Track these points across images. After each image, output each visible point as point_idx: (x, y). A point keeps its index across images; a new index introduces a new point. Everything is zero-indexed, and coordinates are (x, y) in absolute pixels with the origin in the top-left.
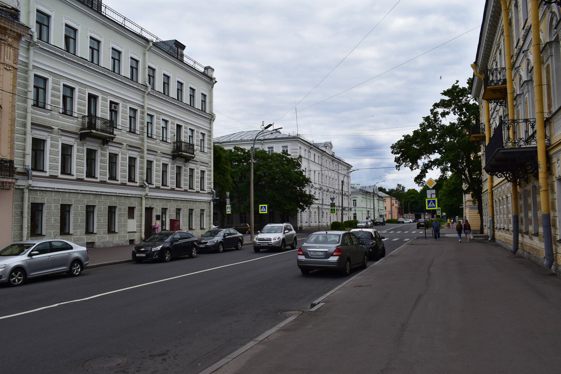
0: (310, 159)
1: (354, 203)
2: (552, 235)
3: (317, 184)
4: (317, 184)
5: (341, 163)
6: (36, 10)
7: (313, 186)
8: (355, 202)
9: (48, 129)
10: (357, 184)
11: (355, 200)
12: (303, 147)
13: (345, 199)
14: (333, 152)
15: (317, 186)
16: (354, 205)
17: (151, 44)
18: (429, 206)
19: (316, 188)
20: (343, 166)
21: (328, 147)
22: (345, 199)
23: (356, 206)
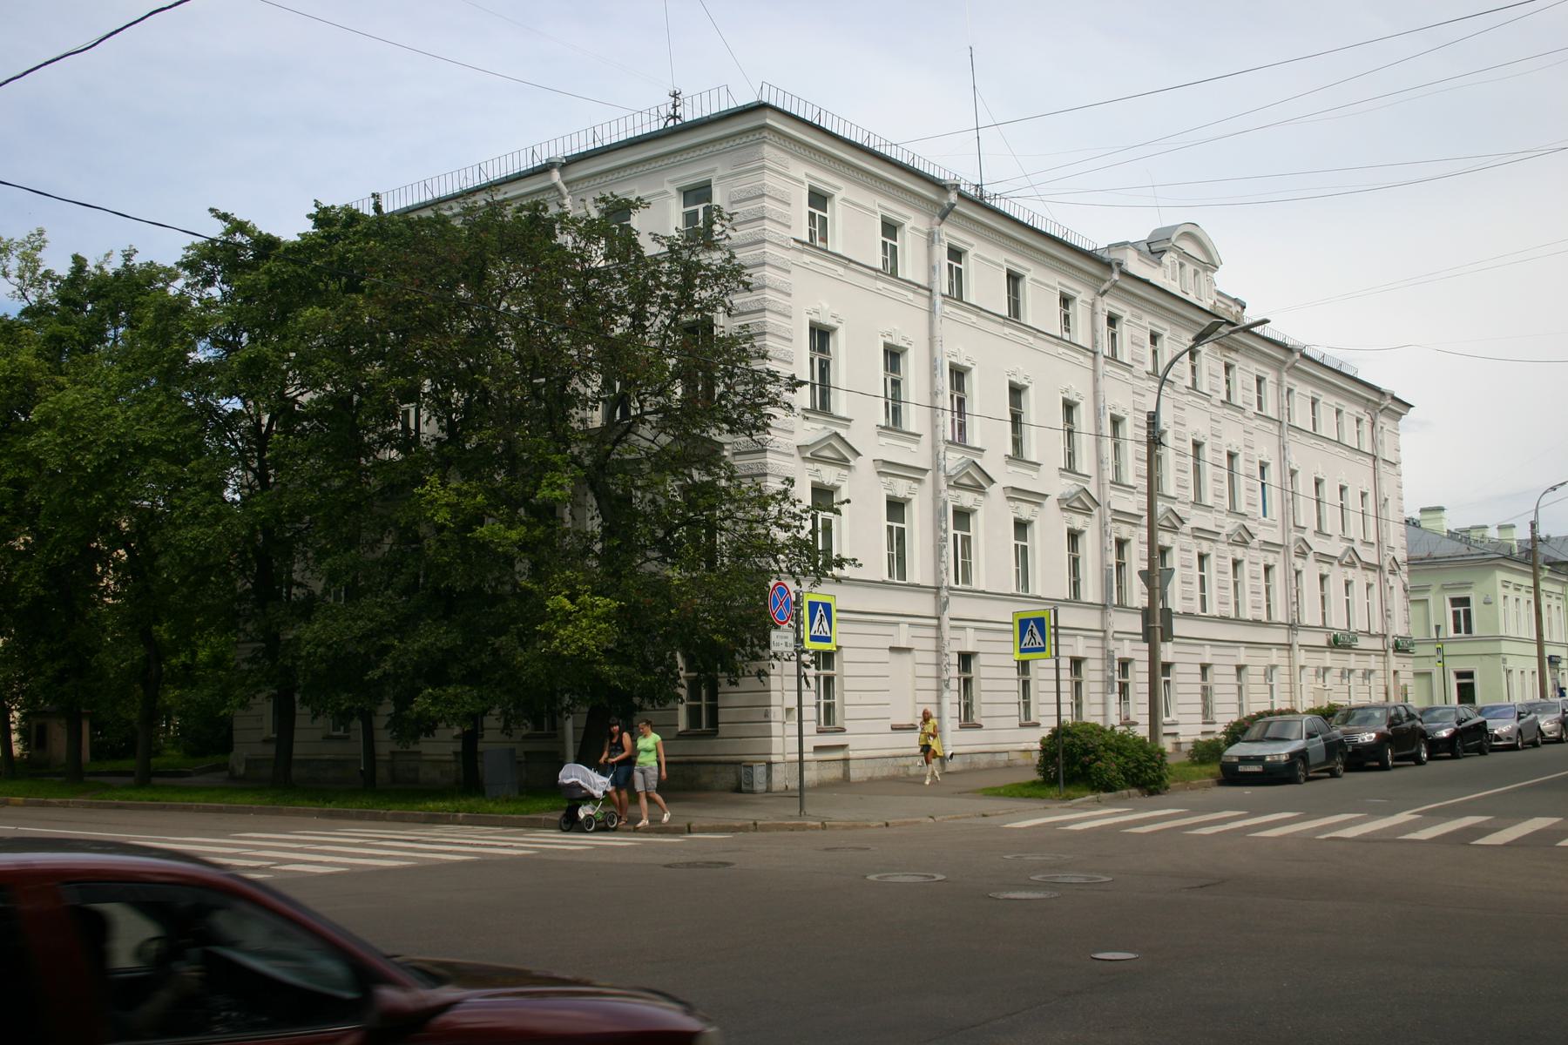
0: (1380, 455)
1: (1456, 614)
2: (1146, 513)
3: (1336, 538)
4: (1336, 538)
5: (1293, 367)
6: (946, 250)
7: (1310, 549)
8: (1461, 609)
9: (1037, 498)
10: (1500, 528)
11: (1465, 601)
12: (1351, 410)
13: (1549, 606)
14: (1236, 301)
15: (1336, 548)
16: (1457, 629)
17: (1297, 356)
18: (1023, 646)
19: (1323, 558)
20: (1348, 400)
21: (1166, 259)
22: (1549, 606)
23: (1469, 630)
